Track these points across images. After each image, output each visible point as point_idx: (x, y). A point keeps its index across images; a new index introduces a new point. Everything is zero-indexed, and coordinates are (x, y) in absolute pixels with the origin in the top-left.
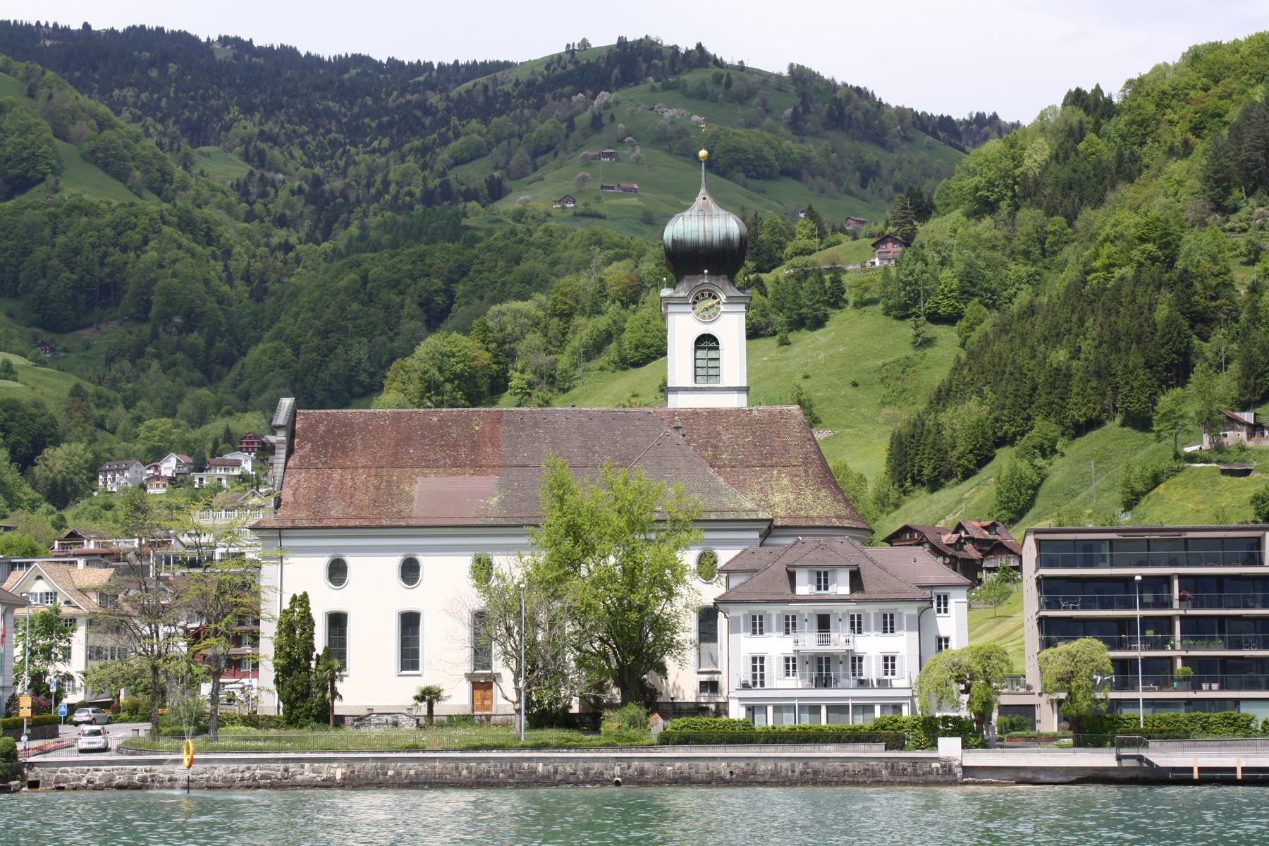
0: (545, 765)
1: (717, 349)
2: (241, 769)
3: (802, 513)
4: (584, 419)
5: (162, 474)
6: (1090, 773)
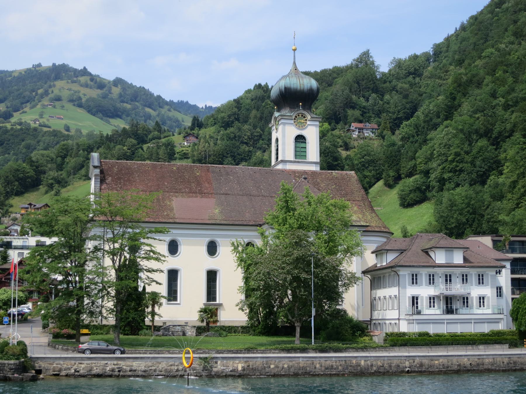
0: (365, 361)
1: (305, 142)
2: (176, 364)
4: (251, 173)
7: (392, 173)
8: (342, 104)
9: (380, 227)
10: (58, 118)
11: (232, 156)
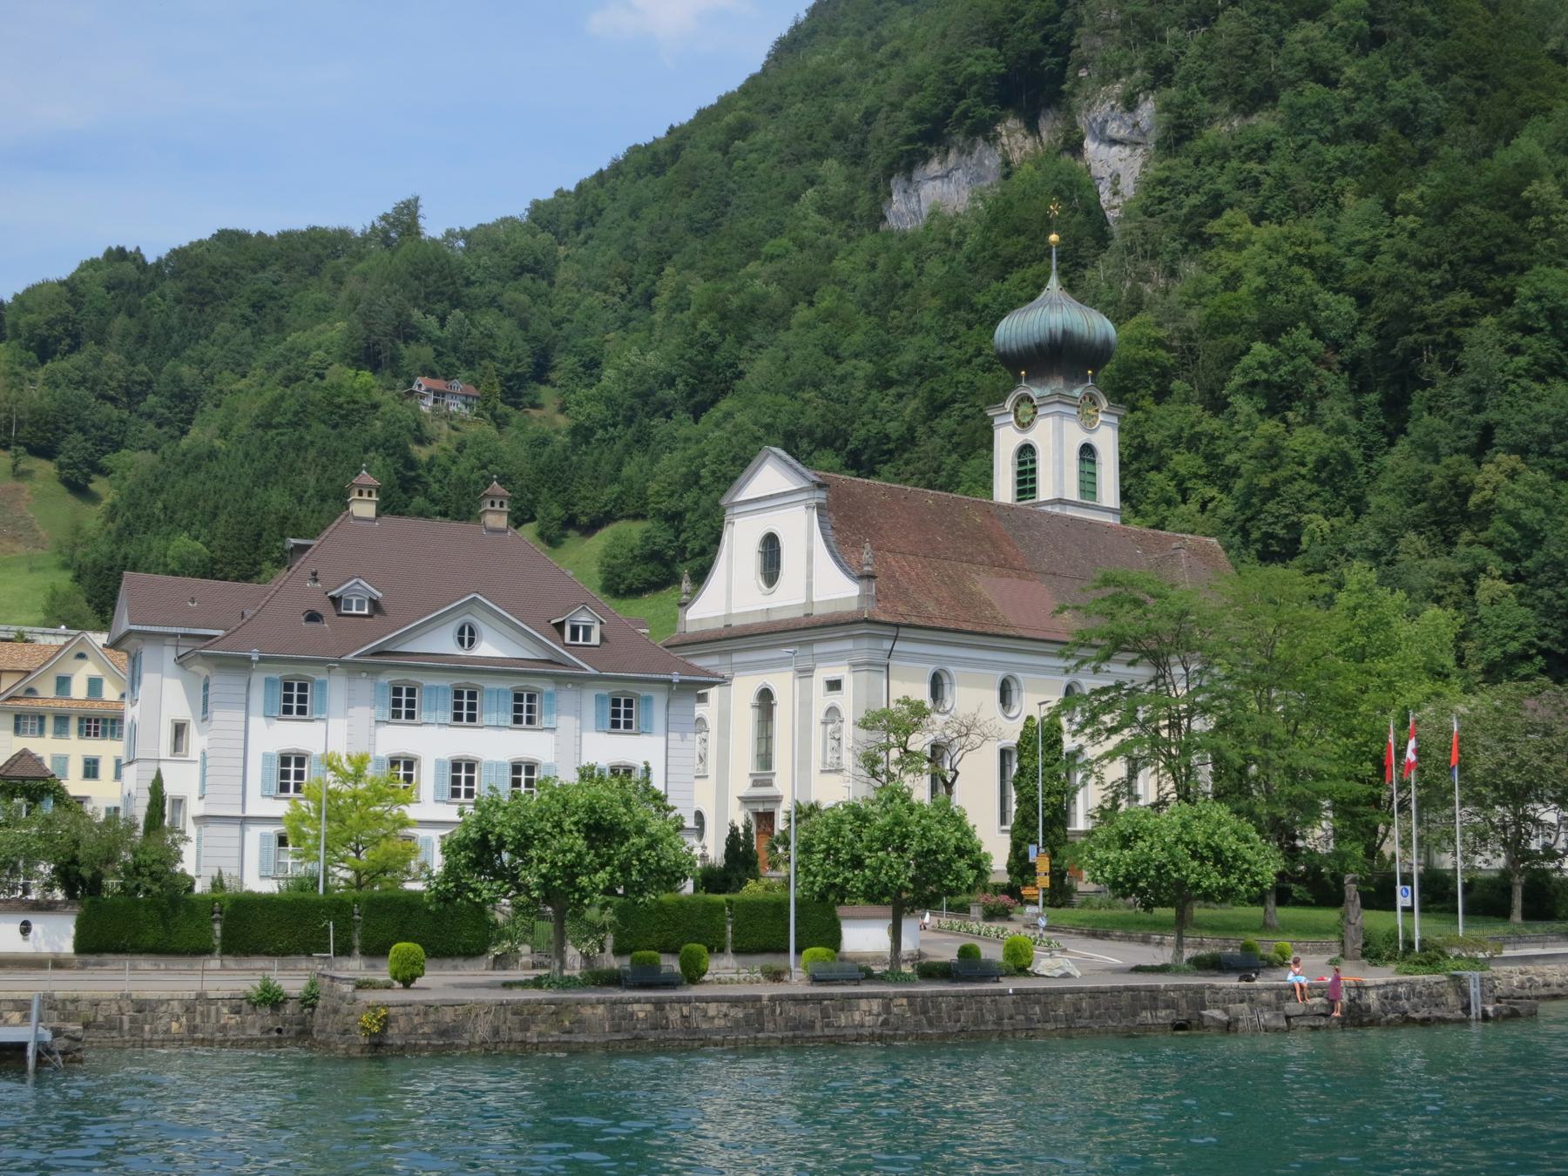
1: (1093, 462)
7: (557, 511)
8: (390, 328)
11: (80, 429)
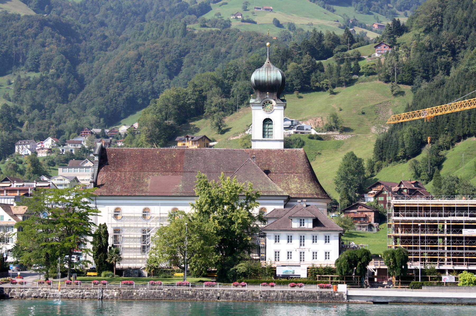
1: (272, 124)
3: (302, 192)
5: (45, 147)
6: (395, 300)
9: (312, 194)
10: (266, 9)
